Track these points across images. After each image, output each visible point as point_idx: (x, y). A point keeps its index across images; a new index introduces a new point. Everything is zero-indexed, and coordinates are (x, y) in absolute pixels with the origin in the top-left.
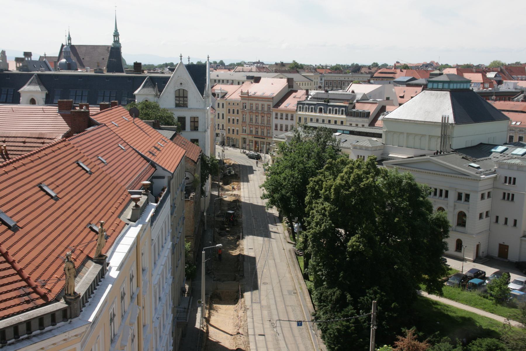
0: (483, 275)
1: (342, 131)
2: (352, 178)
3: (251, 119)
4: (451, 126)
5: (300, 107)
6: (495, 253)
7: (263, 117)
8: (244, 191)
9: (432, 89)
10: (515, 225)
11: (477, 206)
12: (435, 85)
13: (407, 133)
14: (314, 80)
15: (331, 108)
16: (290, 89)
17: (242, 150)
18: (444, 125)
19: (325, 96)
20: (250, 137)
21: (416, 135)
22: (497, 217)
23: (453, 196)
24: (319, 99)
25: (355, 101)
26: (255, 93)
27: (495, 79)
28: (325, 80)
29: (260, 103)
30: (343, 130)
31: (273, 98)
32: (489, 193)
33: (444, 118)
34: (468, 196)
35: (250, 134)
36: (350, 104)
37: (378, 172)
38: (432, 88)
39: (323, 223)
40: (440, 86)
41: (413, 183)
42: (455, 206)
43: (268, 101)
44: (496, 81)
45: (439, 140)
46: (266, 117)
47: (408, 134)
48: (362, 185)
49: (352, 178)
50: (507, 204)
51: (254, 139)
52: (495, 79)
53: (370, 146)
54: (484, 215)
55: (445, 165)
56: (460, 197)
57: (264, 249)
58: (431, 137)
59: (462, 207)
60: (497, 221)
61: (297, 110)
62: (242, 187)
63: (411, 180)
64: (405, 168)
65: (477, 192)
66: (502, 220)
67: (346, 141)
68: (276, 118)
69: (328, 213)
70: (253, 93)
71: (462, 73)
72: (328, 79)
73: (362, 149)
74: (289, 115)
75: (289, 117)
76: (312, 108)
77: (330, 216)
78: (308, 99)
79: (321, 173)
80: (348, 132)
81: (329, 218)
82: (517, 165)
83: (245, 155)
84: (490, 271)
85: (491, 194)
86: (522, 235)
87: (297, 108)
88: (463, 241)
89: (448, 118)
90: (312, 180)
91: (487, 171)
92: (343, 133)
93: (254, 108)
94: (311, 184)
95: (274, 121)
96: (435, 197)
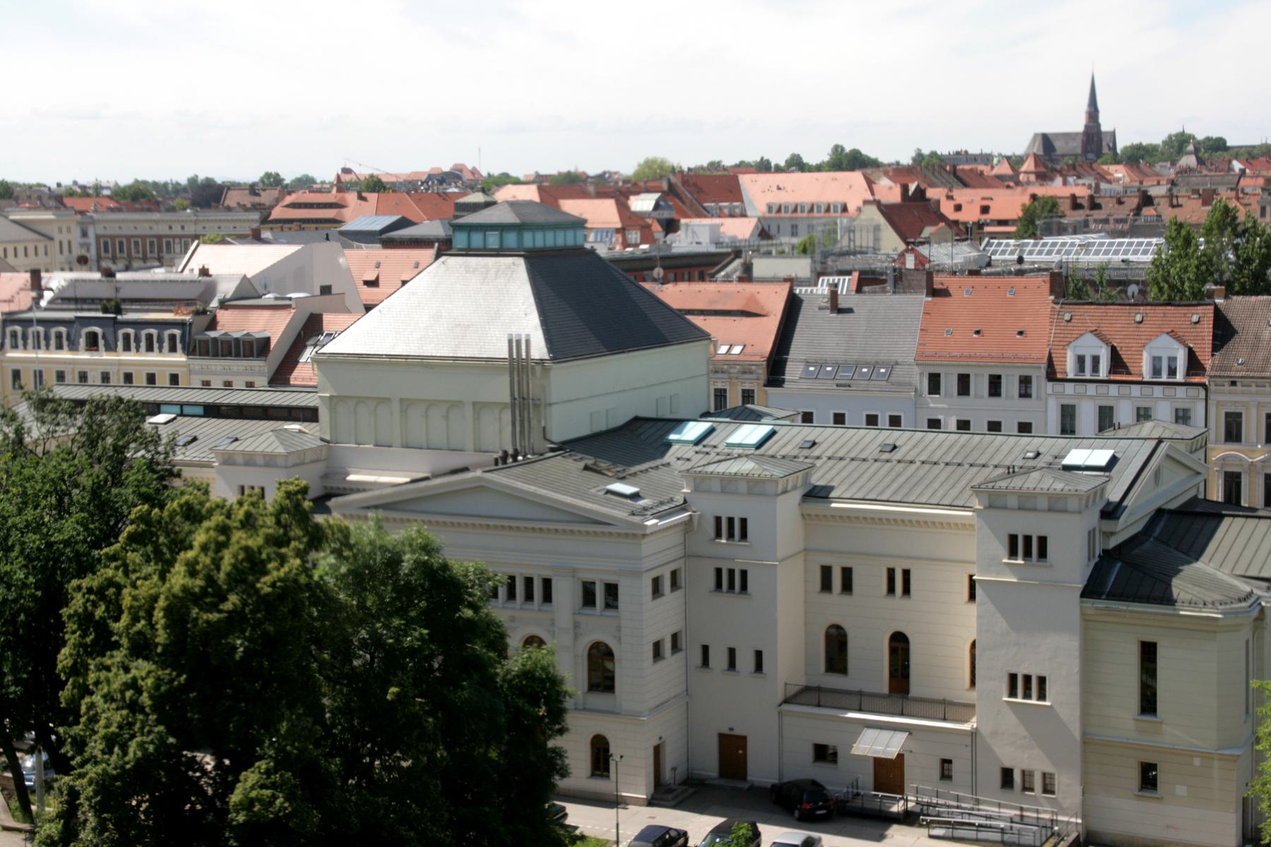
0: (681, 841)
1: (177, 409)
2: (227, 559)
6: (709, 765)
9: (468, 252)
10: (759, 667)
11: (646, 618)
12: (477, 240)
13: (402, 400)
14: (57, 237)
18: (517, 365)
19: (106, 292)
21: (431, 404)
22: (705, 649)
23: (567, 594)
28: (98, 237)
37: (316, 538)
39: (133, 737)
40: (493, 240)
41: (436, 561)
42: (576, 626)
44: (659, 221)
45: (507, 416)
49: (227, 559)
52: (656, 214)
53: (281, 450)
58: (479, 407)
59: (598, 627)
65: (637, 574)
66: (718, 658)
67: (195, 439)
69: (151, 697)
73: (255, 465)
77: (155, 708)
78: (43, 303)
80: (200, 410)
81: (153, 717)
82: (746, 478)
85: (682, 578)
89: (528, 342)
90: (79, 588)
91: (662, 503)
92: (182, 414)
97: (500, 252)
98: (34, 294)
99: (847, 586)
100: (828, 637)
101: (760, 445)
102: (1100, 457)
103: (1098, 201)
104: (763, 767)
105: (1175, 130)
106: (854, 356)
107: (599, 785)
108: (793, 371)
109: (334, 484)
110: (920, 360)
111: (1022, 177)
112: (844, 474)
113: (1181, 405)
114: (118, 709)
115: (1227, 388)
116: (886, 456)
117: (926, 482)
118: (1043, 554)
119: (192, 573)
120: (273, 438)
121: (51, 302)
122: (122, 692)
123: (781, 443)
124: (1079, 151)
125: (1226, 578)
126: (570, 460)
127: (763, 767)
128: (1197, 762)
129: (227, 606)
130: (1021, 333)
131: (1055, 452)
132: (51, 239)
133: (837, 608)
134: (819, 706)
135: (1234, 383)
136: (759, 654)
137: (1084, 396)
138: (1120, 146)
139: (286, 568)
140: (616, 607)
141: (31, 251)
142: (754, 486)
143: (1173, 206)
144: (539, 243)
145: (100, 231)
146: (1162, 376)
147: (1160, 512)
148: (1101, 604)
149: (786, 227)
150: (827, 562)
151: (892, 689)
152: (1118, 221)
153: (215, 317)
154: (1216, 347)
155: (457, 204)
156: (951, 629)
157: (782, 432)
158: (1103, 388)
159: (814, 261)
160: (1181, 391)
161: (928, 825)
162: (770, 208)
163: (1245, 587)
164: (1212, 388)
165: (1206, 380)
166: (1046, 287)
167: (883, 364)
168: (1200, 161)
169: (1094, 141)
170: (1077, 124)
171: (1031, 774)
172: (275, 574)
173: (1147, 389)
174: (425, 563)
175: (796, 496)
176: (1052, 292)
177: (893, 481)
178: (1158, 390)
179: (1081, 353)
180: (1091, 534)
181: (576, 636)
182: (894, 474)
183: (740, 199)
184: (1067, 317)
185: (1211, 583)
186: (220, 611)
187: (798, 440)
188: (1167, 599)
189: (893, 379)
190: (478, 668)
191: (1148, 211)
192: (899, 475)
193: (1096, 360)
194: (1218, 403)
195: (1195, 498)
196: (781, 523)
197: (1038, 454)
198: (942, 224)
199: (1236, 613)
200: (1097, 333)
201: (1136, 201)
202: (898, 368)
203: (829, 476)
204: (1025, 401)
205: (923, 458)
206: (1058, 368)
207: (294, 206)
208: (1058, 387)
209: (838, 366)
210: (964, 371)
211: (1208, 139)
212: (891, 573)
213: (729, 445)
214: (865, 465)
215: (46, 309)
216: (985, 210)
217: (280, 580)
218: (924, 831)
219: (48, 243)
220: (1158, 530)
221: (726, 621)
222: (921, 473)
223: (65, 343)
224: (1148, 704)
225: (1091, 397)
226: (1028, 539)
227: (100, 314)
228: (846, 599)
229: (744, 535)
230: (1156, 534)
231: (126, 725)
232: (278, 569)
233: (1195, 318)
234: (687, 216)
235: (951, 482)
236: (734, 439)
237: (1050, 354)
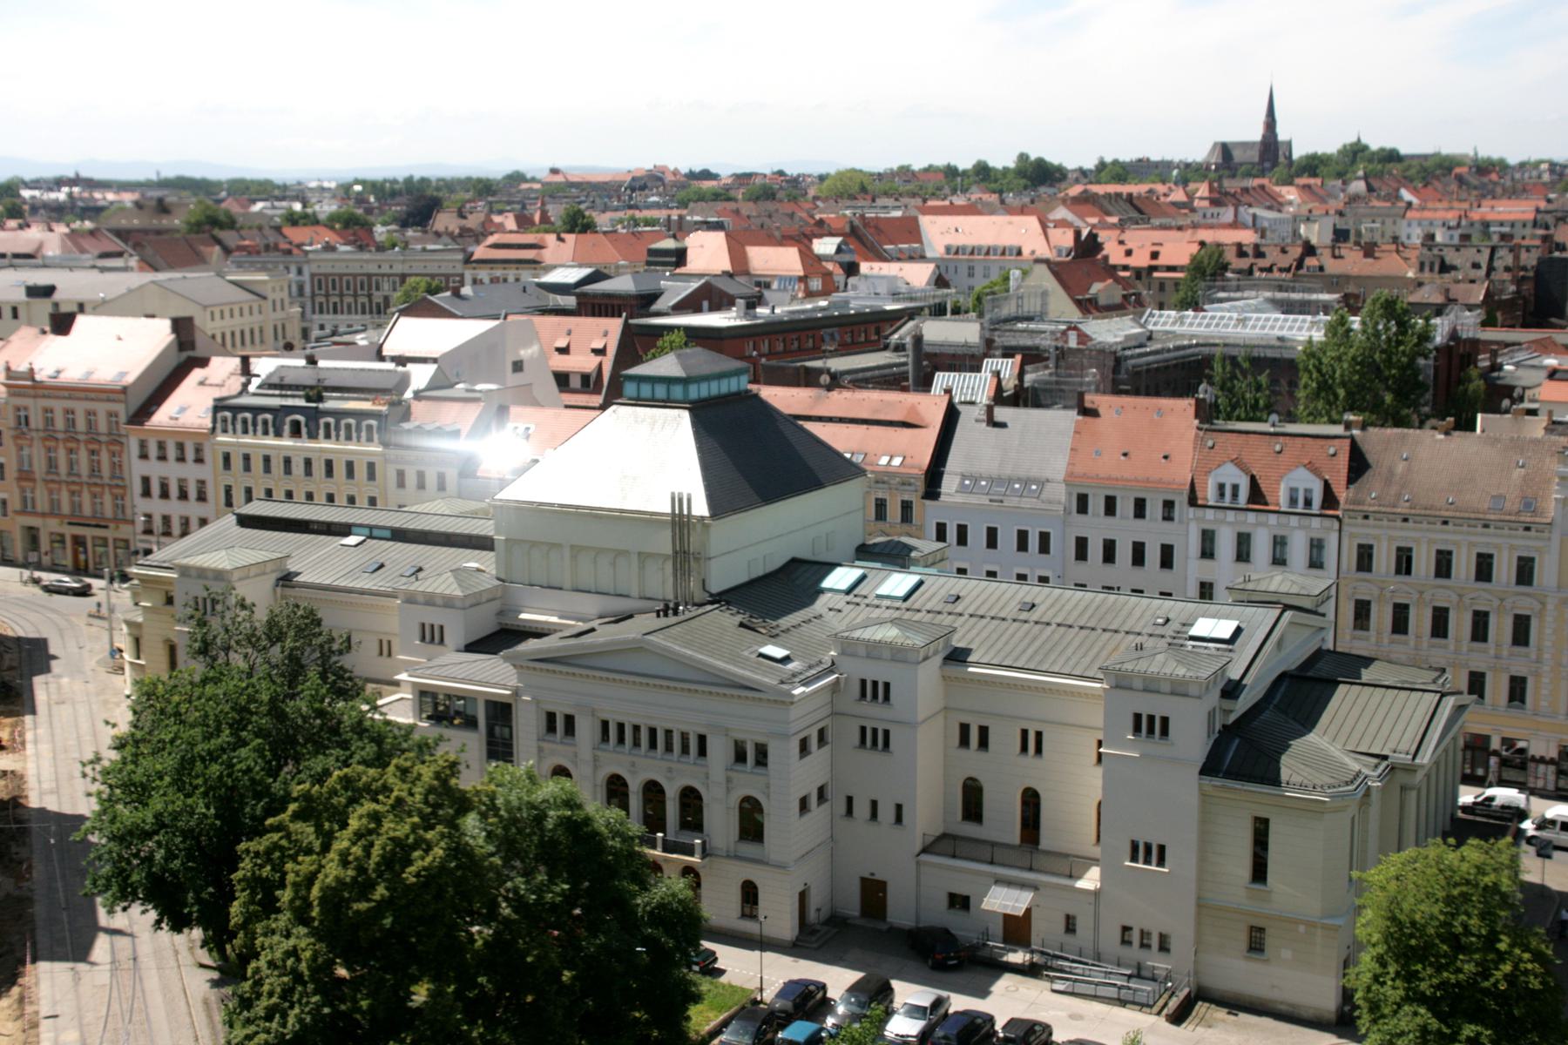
0: (820, 995)
1: (366, 531)
2: (376, 852)
3: (52, 464)
4: (699, 527)
5: (225, 420)
6: (852, 905)
7: (93, 452)
8: (37, 755)
9: (638, 401)
10: (899, 819)
11: (794, 775)
12: (646, 390)
13: (572, 547)
14: (271, 296)
15: (331, 420)
16: (185, 355)
17: (26, 573)
18: (680, 522)
19: (308, 378)
20: (53, 525)
21: (600, 551)
22: (850, 800)
23: (720, 751)
24: (290, 387)
25: (408, 395)
26: (58, 372)
27: (838, 258)
28: (313, 276)
29: (80, 407)
30: (371, 527)
31: (125, 390)
32: (821, 733)
33: (676, 500)
35: (52, 514)
36: (392, 404)
37: (463, 804)
38: (638, 398)
39: (292, 1007)
40: (661, 392)
41: (579, 815)
42: (729, 780)
43: (109, 400)
44: (841, 265)
45: (669, 567)
47: (576, 550)
48: (409, 875)
49: (376, 852)
50: (872, 759)
51: (69, 531)
52: (838, 258)
53: (458, 593)
55: (690, 658)
56: (740, 756)
57: (115, 1007)
58: (643, 557)
59: (748, 783)
61: (214, 429)
62: (29, 736)
63: (571, 808)
64: (571, 670)
65: (786, 736)
66: (863, 810)
67: (382, 566)
68: (144, 456)
69: (309, 968)
70: (50, 371)
71: (743, 246)
72: (322, 271)
73: (434, 605)
74: (187, 447)
75: (190, 454)
76: (265, 422)
77: (313, 979)
78: (252, 388)
79: (278, 828)
80: (387, 534)
81: (310, 987)
82: (889, 645)
83: (36, 590)
84: (838, 980)
85: (829, 736)
86: (918, 847)
87: (214, 421)
88: (758, 883)
89: (689, 501)
90: (247, 851)
91: (810, 667)
92: (371, 537)
93: (60, 424)
94: (246, 865)
95: (138, 469)
96: (668, 756)
97: (667, 403)
98: (243, 379)
99: (984, 743)
100: (965, 786)
101: (906, 598)
102: (1225, 629)
103: (1263, 249)
104: (900, 912)
105: (1351, 139)
106: (1008, 471)
107: (749, 926)
108: (949, 484)
109: (508, 621)
110: (1069, 480)
111: (1196, 203)
112: (984, 634)
113: (1316, 535)
114: (279, 976)
115: (1360, 520)
116: (1024, 616)
117: (1060, 648)
118: (1165, 732)
119: (344, 861)
120: (452, 579)
121: (260, 387)
122: (284, 961)
123: (927, 595)
124: (1256, 159)
125: (1337, 754)
126: (727, 614)
127: (900, 912)
128: (1302, 928)
129: (377, 896)
130: (1166, 457)
131: (1183, 619)
132: (265, 298)
133: (973, 763)
134: (954, 856)
135: (1366, 517)
136: (899, 807)
137: (1223, 522)
138: (1296, 155)
139: (429, 859)
140: (765, 765)
141: (246, 311)
142: (897, 654)
143: (1334, 257)
144: (704, 393)
145: (314, 269)
146: (1300, 505)
147: (1283, 676)
148: (1218, 782)
149: (963, 270)
150: (965, 720)
151: (1023, 839)
152: (1281, 270)
153: (409, 407)
154: (1351, 480)
155: (652, 252)
156: (1077, 789)
157: (929, 581)
158: (1241, 516)
159: (982, 328)
160: (1316, 522)
161: (1052, 979)
162: (948, 249)
163: (1354, 765)
164: (1346, 520)
165: (1339, 513)
166: (1192, 410)
167: (1035, 481)
168: (1370, 189)
169: (1271, 149)
170: (1256, 134)
171: (1149, 934)
172: (420, 863)
173: (1283, 518)
174: (569, 818)
175: (938, 660)
176: (1197, 416)
177: (1029, 645)
178: (1294, 520)
179: (1222, 480)
180: (1211, 715)
181: (728, 790)
182: (1030, 636)
183: (919, 239)
184: (1210, 443)
185: (1321, 761)
186: (368, 900)
187: (943, 592)
188: (1275, 781)
189: (1043, 496)
190: (621, 904)
191: (1311, 262)
192: (1035, 639)
193: (1235, 488)
194: (1352, 536)
195: (1319, 654)
196: (923, 690)
197: (1168, 620)
198: (1110, 281)
199: (1343, 795)
200: (1238, 463)
201: (1299, 250)
202: (1048, 486)
203: (970, 636)
204: (1167, 524)
205: (1059, 620)
206: (1199, 494)
207: (496, 246)
208: (1199, 512)
209: (991, 480)
210: (1111, 493)
211: (1382, 150)
212: (1025, 733)
213: (879, 597)
214: (1005, 624)
215: (254, 394)
216: (1155, 255)
217: (425, 869)
218: (1046, 985)
219: (262, 302)
220: (1278, 696)
221: (870, 776)
222: (1057, 636)
223: (271, 430)
224: (1259, 872)
225: (1230, 523)
226: (1151, 718)
227: (302, 403)
228: (982, 755)
229: (887, 698)
230: (1275, 702)
231: (286, 993)
232: (423, 858)
233: (1332, 451)
234: (867, 260)
235: (1083, 650)
236: (882, 591)
237: (1192, 485)
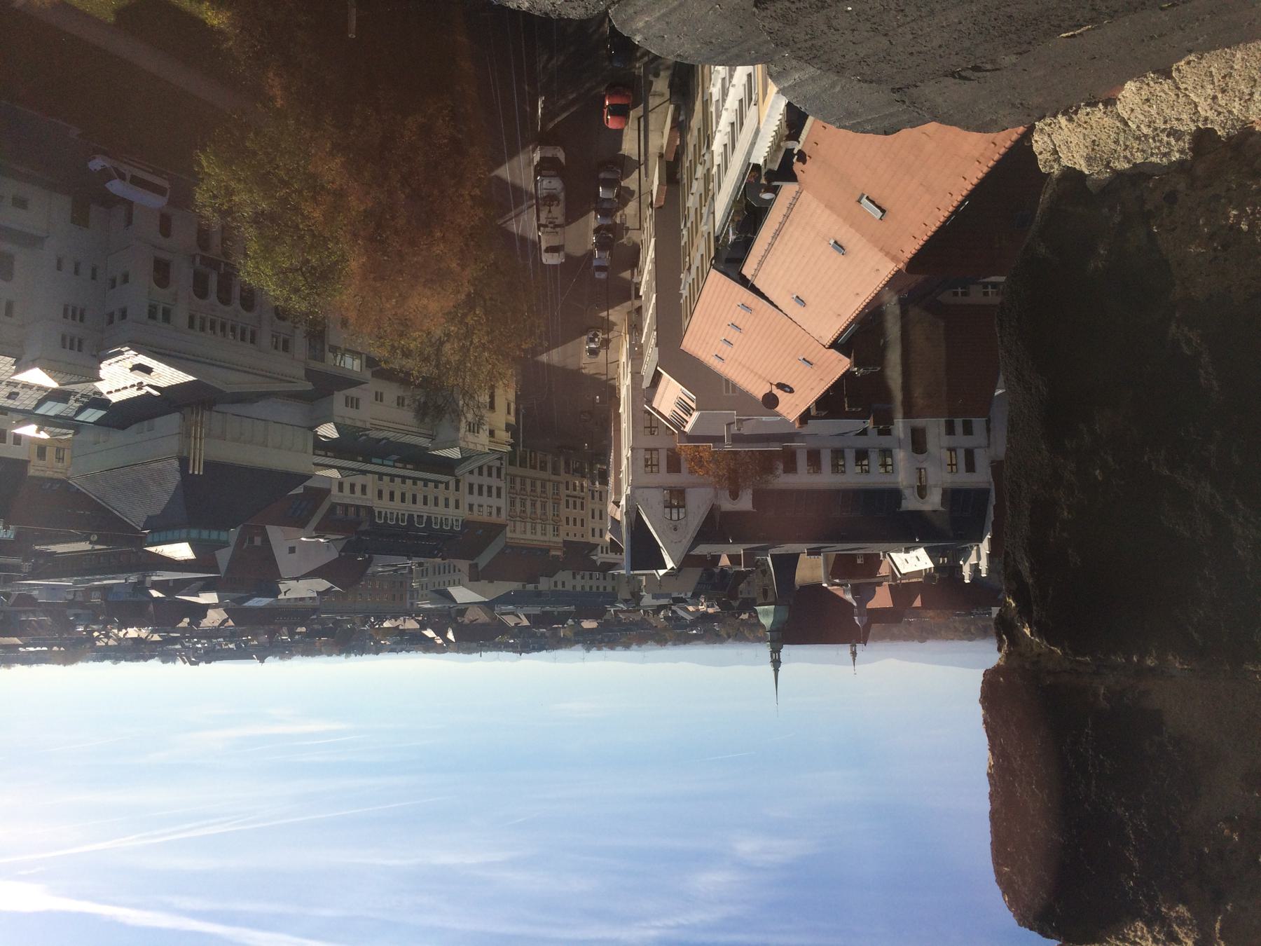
10: (59, 262)
34: (152, 315)
46: (518, 510)
54: (116, 317)
56: (167, 315)
60: (94, 270)
